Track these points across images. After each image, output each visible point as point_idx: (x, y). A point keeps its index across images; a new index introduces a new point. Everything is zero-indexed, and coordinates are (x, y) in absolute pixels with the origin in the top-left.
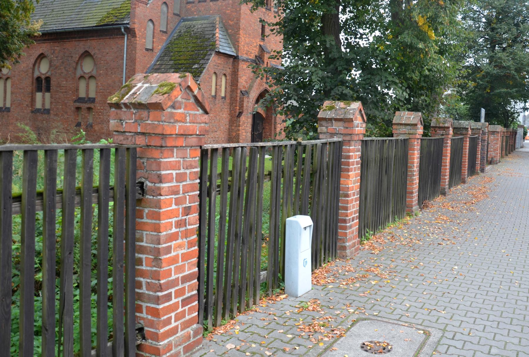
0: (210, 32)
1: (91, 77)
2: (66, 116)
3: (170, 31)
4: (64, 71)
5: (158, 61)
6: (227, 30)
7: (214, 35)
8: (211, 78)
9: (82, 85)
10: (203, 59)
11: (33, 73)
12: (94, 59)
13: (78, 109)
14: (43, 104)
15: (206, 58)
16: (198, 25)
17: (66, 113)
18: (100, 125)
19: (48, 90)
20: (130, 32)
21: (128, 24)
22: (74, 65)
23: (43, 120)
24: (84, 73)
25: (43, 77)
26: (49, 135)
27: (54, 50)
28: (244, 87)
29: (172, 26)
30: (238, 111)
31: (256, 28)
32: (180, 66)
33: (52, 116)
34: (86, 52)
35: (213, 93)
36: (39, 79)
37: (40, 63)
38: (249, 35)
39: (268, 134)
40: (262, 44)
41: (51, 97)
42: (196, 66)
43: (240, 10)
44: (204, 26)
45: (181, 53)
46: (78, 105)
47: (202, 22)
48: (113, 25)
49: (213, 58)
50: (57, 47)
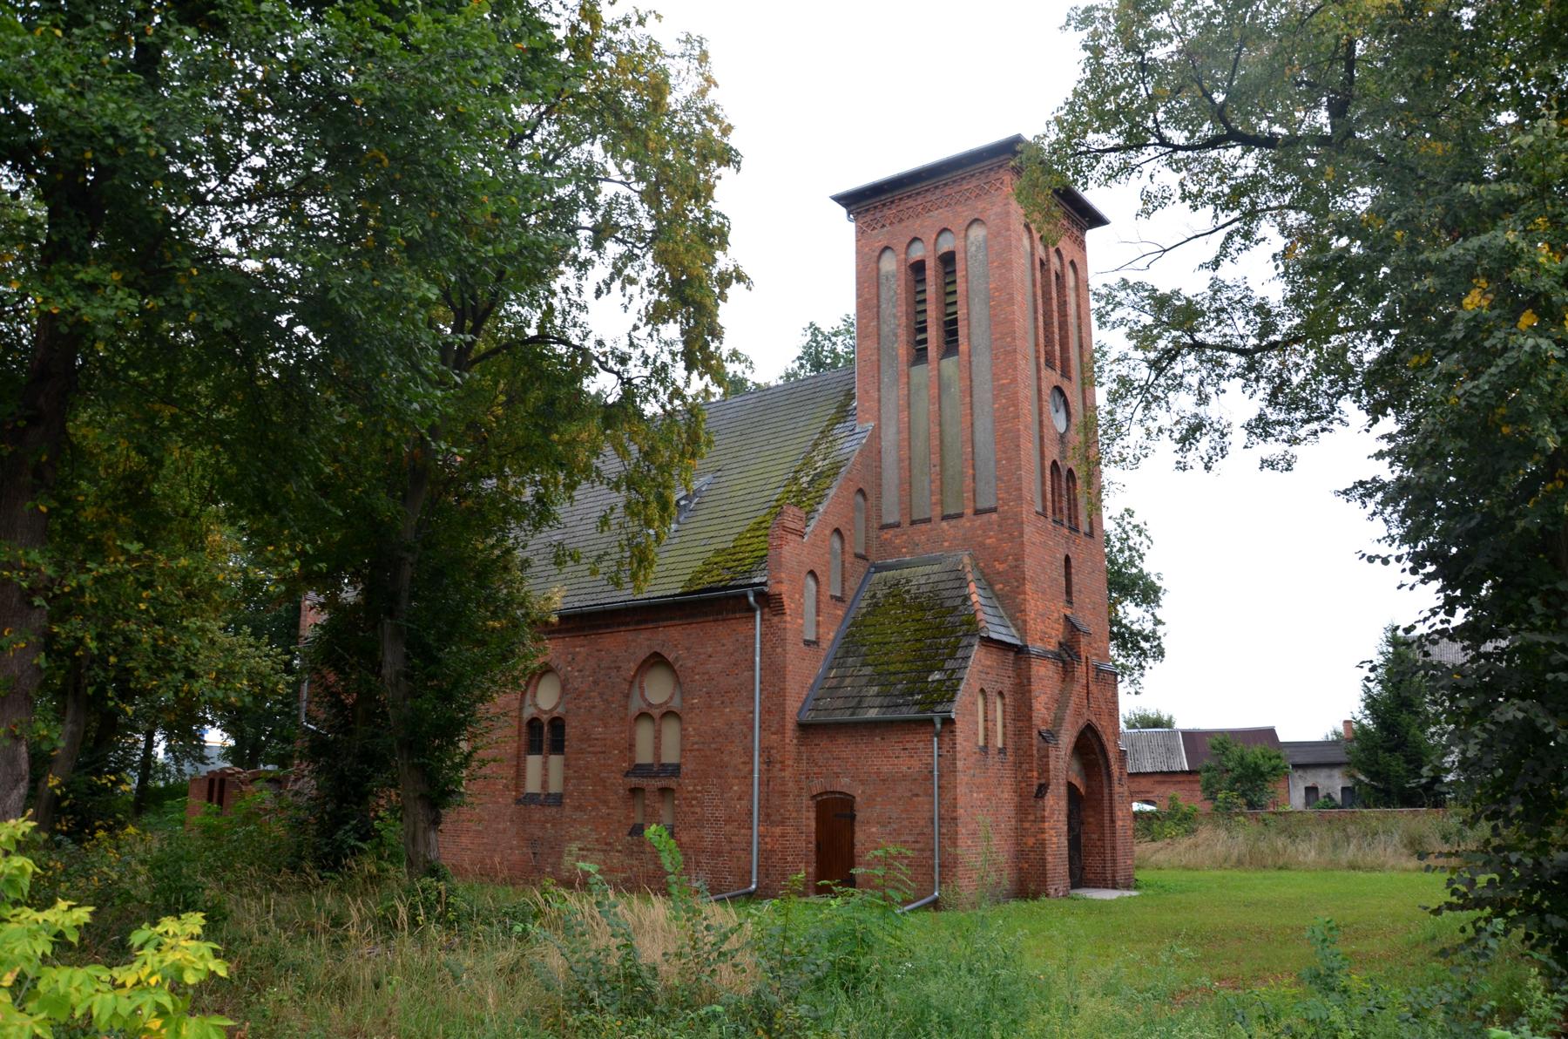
0: (955, 593)
1: (669, 714)
2: (604, 810)
3: (850, 594)
4: (597, 701)
5: (831, 668)
6: (991, 585)
7: (967, 598)
8: (975, 704)
9: (644, 733)
10: (952, 657)
11: (521, 709)
12: (674, 671)
13: (635, 791)
14: (544, 784)
15: (959, 654)
16: (919, 577)
17: (606, 803)
18: (694, 832)
19: (558, 747)
20: (770, 602)
21: (764, 584)
22: (625, 686)
23: (547, 822)
24: (650, 705)
25: (545, 718)
26: (560, 857)
27: (575, 655)
28: (1045, 722)
29: (853, 583)
30: (1036, 782)
31: (1055, 575)
32: (892, 678)
33: (568, 811)
34: (656, 654)
35: (981, 743)
36: (534, 724)
37: (536, 687)
38: (1044, 593)
39: (1095, 836)
40: (1068, 613)
41: (567, 766)
42: (936, 676)
43: (1022, 534)
44: (934, 578)
45: (889, 647)
46: (635, 781)
47: (928, 569)
48: (725, 588)
49: (977, 653)
50: (581, 647)
